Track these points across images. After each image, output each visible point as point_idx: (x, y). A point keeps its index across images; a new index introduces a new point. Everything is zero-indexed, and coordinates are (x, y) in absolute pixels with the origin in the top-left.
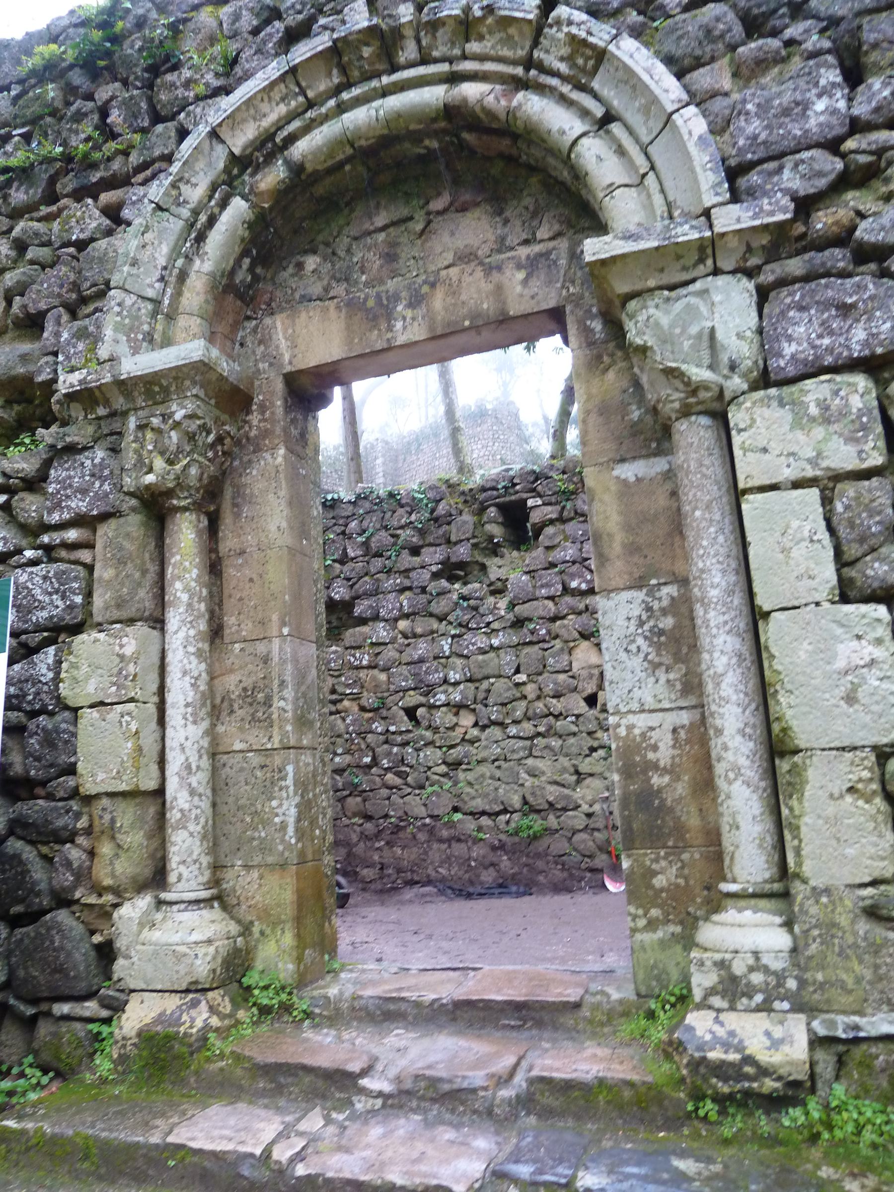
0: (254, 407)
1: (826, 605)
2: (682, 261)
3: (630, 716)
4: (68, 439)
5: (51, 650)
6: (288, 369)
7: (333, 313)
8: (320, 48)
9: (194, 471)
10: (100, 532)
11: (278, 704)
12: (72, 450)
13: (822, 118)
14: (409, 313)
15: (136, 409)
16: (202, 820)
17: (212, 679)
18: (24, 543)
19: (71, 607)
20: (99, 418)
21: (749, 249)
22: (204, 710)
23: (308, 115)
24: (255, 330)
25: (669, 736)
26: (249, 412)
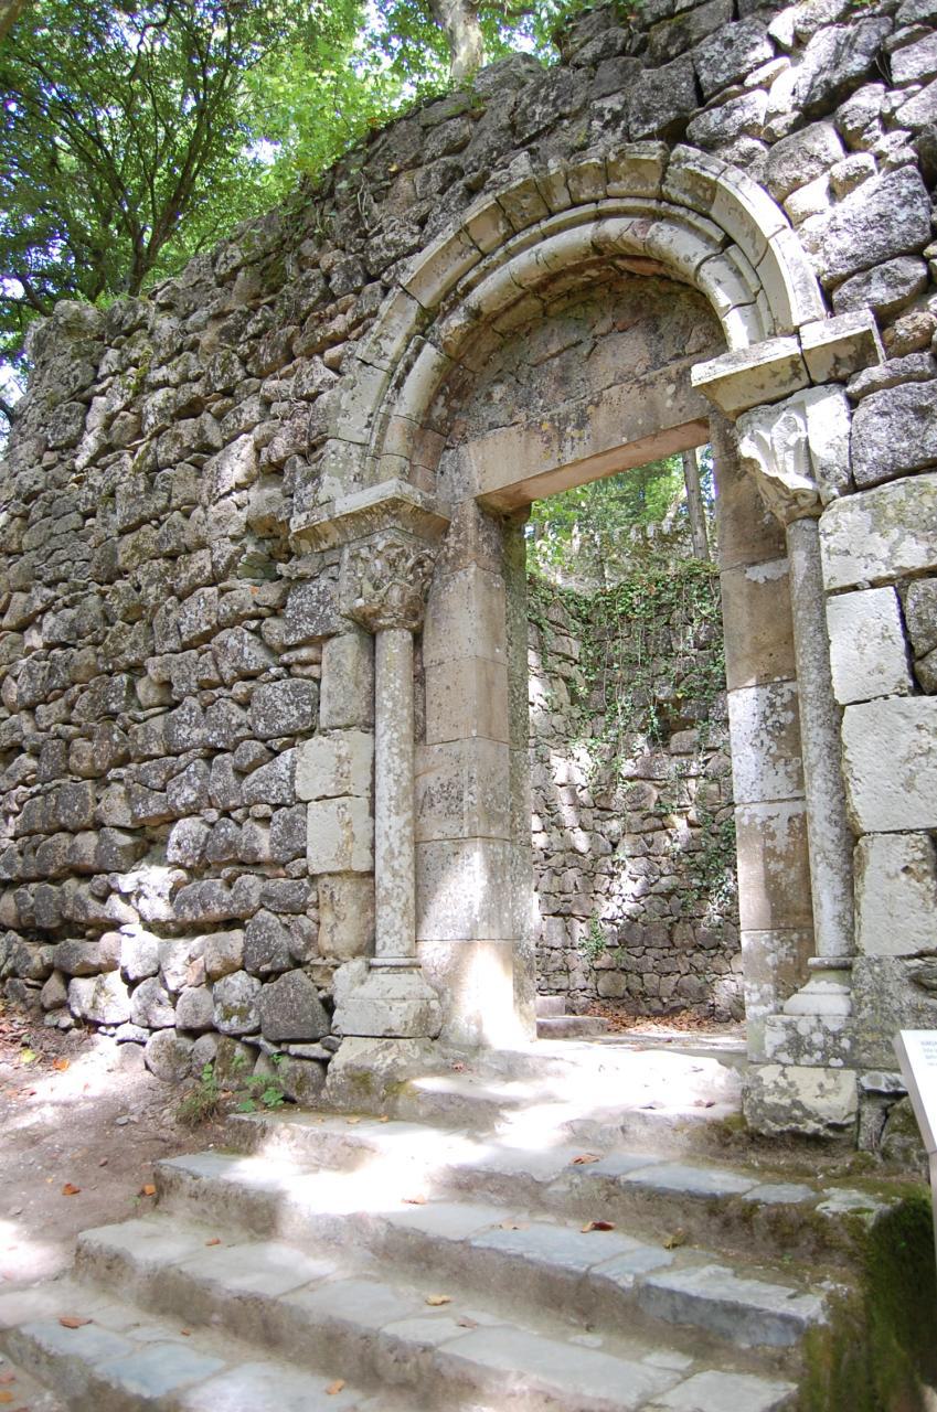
0: (451, 530)
1: (894, 698)
2: (778, 377)
3: (753, 806)
4: (299, 571)
5: (289, 752)
6: (479, 492)
7: (516, 438)
8: (485, 207)
9: (396, 593)
10: (325, 650)
11: (467, 798)
12: (302, 579)
13: (904, 227)
14: (575, 434)
15: (349, 543)
16: (403, 899)
17: (416, 777)
18: (270, 663)
19: (303, 716)
20: (323, 552)
21: (838, 360)
22: (405, 804)
23: (482, 265)
24: (452, 459)
25: (786, 825)
26: (446, 534)
